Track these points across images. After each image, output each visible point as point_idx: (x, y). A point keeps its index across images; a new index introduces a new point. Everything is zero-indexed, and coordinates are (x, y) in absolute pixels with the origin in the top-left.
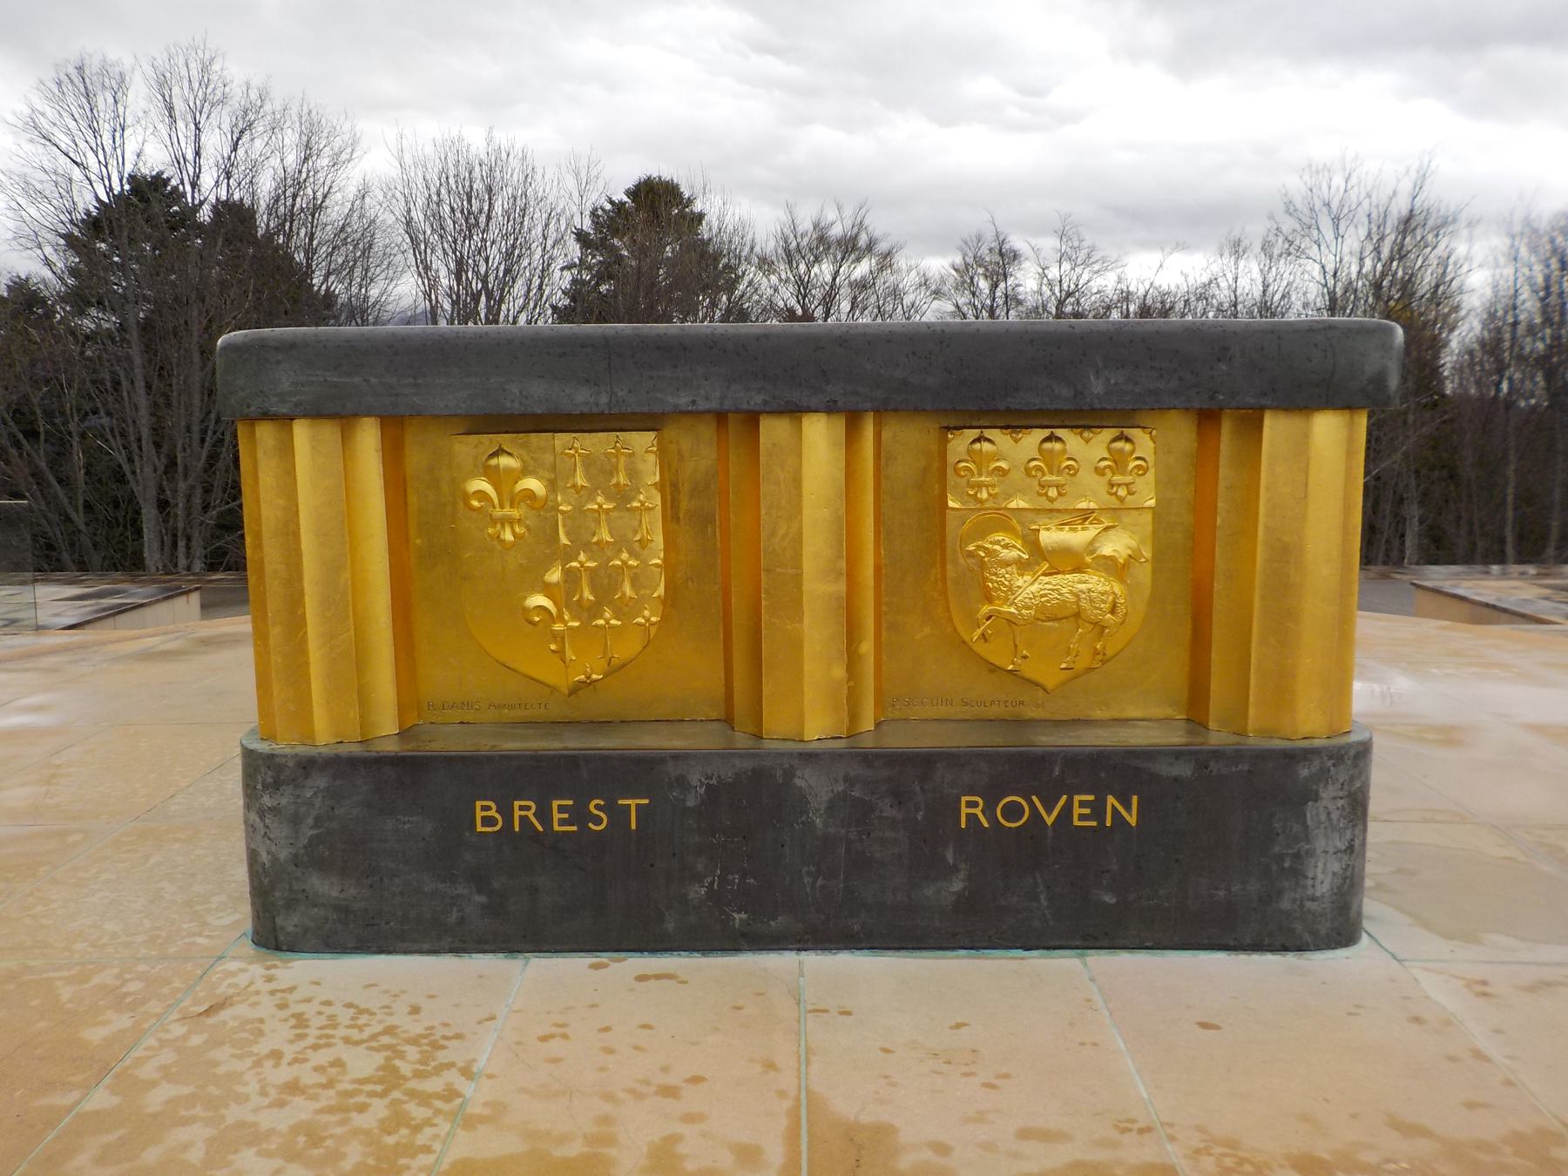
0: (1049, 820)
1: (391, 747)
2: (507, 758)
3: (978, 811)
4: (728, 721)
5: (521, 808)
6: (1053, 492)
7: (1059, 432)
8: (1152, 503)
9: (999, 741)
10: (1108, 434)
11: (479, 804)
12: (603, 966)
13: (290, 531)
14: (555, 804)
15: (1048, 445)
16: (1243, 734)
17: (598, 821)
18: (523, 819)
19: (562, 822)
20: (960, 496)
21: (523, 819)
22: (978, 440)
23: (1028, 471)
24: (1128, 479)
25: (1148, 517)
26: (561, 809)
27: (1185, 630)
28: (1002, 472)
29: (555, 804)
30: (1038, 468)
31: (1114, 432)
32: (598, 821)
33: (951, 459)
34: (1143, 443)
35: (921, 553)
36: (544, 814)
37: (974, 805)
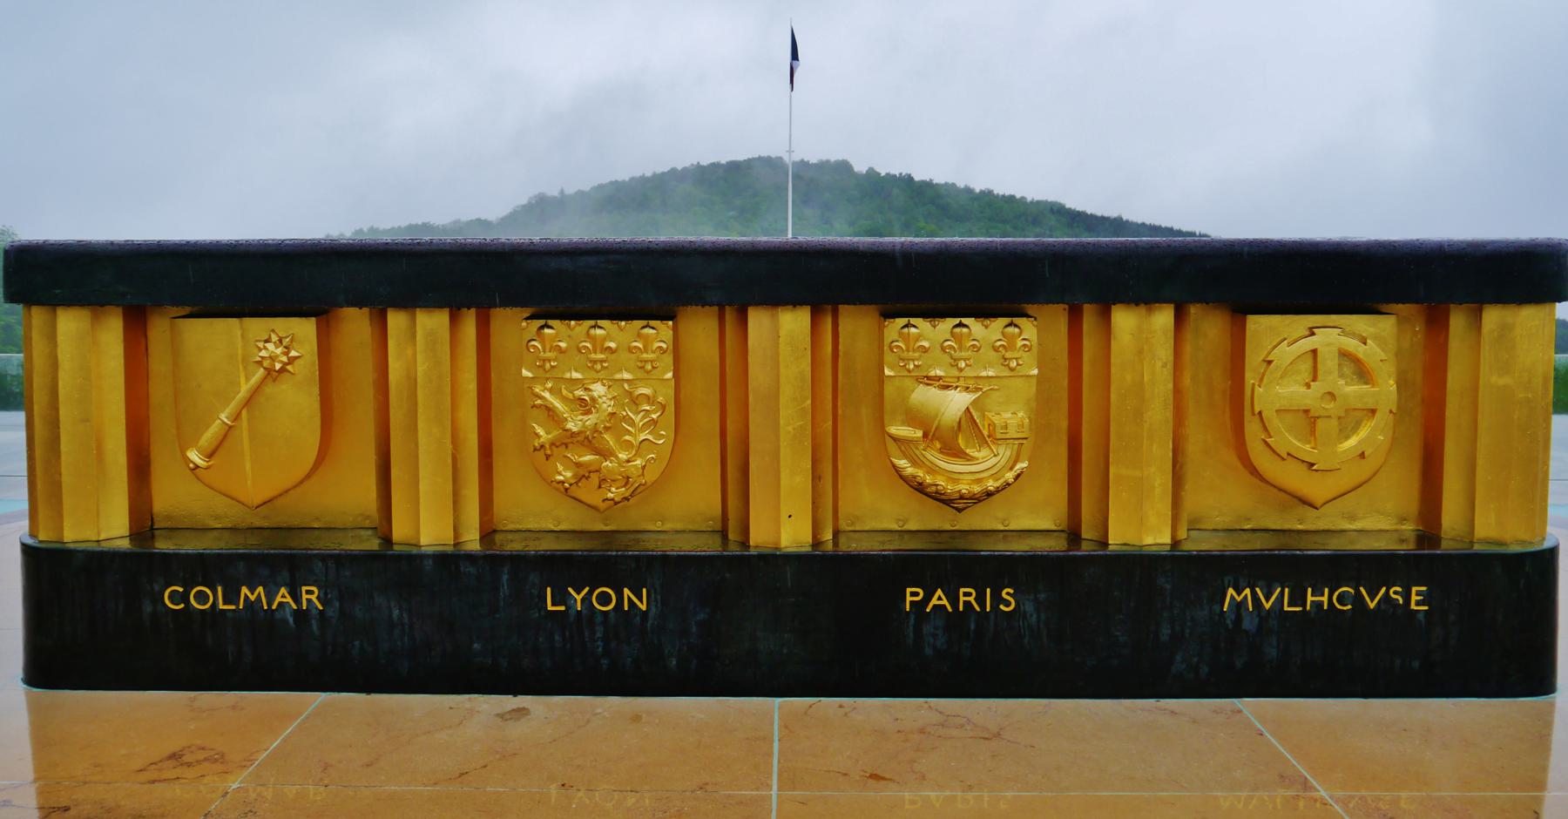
0: (1268, 606)
1: (125, 544)
2: (187, 556)
3: (971, 599)
4: (724, 533)
5: (308, 592)
6: (962, 364)
7: (965, 321)
8: (1035, 372)
9: (577, 547)
10: (1003, 321)
11: (909, 590)
12: (521, 712)
13: (774, 395)
14: (1414, 589)
15: (958, 330)
16: (1105, 544)
17: (1008, 604)
18: (309, 601)
19: (1418, 603)
20: (891, 368)
21: (309, 601)
22: (1010, 325)
23: (943, 349)
24: (1016, 355)
25: (1034, 381)
26: (1418, 594)
27: (807, 464)
28: (925, 350)
29: (1414, 589)
30: (951, 347)
31: (1006, 320)
32: (1008, 604)
33: (887, 341)
34: (1028, 330)
35: (845, 412)
36: (1407, 596)
37: (969, 594)
